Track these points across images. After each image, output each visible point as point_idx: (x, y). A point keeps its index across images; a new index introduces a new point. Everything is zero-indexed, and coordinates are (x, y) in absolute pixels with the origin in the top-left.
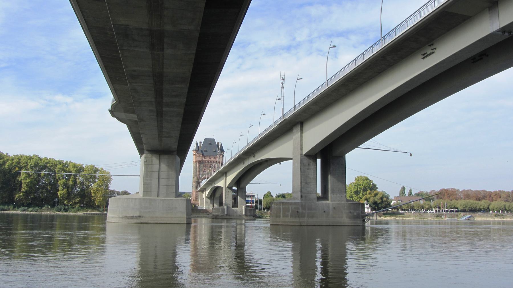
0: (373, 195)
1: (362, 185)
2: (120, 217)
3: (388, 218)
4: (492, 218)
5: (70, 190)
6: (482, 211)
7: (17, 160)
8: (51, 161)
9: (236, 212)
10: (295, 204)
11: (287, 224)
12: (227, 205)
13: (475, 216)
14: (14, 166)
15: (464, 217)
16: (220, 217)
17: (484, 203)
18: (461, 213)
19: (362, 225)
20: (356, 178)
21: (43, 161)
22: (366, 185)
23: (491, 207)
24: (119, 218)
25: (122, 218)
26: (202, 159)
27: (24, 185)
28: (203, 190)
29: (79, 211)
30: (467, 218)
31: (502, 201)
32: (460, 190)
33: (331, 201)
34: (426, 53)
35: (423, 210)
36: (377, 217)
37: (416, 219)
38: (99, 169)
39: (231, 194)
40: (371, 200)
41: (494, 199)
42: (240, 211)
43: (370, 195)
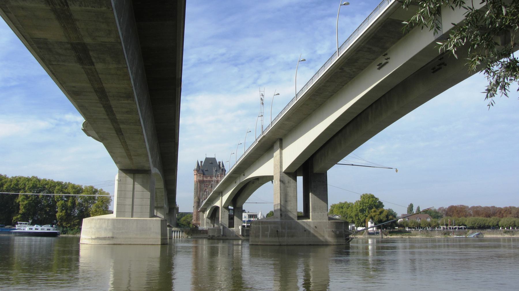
0: (378, 213)
1: (368, 203)
2: (93, 238)
3: (394, 237)
4: (501, 235)
5: (69, 212)
6: (491, 228)
7: (15, 182)
8: (49, 182)
9: (233, 232)
10: (275, 223)
11: (266, 244)
12: (223, 225)
13: (484, 233)
14: (13, 187)
15: (472, 235)
16: (216, 237)
17: (494, 219)
18: (469, 230)
19: (345, 244)
20: (361, 196)
21: (41, 183)
22: (372, 203)
23: (500, 224)
24: (92, 239)
25: (95, 239)
26: (203, 179)
27: (21, 207)
28: (204, 211)
29: (78, 233)
30: (475, 235)
31: (512, 217)
32: (470, 207)
33: (312, 220)
34: (381, 64)
35: (430, 228)
36: (382, 235)
37: (423, 237)
38: (98, 190)
39: (227, 214)
40: (376, 218)
41: (504, 215)
42: (237, 231)
43: (375, 213)
